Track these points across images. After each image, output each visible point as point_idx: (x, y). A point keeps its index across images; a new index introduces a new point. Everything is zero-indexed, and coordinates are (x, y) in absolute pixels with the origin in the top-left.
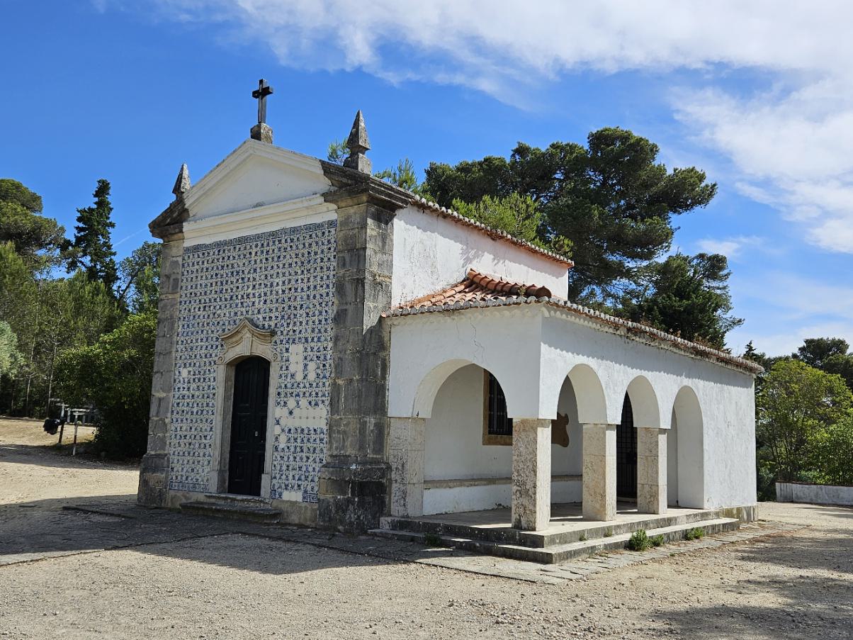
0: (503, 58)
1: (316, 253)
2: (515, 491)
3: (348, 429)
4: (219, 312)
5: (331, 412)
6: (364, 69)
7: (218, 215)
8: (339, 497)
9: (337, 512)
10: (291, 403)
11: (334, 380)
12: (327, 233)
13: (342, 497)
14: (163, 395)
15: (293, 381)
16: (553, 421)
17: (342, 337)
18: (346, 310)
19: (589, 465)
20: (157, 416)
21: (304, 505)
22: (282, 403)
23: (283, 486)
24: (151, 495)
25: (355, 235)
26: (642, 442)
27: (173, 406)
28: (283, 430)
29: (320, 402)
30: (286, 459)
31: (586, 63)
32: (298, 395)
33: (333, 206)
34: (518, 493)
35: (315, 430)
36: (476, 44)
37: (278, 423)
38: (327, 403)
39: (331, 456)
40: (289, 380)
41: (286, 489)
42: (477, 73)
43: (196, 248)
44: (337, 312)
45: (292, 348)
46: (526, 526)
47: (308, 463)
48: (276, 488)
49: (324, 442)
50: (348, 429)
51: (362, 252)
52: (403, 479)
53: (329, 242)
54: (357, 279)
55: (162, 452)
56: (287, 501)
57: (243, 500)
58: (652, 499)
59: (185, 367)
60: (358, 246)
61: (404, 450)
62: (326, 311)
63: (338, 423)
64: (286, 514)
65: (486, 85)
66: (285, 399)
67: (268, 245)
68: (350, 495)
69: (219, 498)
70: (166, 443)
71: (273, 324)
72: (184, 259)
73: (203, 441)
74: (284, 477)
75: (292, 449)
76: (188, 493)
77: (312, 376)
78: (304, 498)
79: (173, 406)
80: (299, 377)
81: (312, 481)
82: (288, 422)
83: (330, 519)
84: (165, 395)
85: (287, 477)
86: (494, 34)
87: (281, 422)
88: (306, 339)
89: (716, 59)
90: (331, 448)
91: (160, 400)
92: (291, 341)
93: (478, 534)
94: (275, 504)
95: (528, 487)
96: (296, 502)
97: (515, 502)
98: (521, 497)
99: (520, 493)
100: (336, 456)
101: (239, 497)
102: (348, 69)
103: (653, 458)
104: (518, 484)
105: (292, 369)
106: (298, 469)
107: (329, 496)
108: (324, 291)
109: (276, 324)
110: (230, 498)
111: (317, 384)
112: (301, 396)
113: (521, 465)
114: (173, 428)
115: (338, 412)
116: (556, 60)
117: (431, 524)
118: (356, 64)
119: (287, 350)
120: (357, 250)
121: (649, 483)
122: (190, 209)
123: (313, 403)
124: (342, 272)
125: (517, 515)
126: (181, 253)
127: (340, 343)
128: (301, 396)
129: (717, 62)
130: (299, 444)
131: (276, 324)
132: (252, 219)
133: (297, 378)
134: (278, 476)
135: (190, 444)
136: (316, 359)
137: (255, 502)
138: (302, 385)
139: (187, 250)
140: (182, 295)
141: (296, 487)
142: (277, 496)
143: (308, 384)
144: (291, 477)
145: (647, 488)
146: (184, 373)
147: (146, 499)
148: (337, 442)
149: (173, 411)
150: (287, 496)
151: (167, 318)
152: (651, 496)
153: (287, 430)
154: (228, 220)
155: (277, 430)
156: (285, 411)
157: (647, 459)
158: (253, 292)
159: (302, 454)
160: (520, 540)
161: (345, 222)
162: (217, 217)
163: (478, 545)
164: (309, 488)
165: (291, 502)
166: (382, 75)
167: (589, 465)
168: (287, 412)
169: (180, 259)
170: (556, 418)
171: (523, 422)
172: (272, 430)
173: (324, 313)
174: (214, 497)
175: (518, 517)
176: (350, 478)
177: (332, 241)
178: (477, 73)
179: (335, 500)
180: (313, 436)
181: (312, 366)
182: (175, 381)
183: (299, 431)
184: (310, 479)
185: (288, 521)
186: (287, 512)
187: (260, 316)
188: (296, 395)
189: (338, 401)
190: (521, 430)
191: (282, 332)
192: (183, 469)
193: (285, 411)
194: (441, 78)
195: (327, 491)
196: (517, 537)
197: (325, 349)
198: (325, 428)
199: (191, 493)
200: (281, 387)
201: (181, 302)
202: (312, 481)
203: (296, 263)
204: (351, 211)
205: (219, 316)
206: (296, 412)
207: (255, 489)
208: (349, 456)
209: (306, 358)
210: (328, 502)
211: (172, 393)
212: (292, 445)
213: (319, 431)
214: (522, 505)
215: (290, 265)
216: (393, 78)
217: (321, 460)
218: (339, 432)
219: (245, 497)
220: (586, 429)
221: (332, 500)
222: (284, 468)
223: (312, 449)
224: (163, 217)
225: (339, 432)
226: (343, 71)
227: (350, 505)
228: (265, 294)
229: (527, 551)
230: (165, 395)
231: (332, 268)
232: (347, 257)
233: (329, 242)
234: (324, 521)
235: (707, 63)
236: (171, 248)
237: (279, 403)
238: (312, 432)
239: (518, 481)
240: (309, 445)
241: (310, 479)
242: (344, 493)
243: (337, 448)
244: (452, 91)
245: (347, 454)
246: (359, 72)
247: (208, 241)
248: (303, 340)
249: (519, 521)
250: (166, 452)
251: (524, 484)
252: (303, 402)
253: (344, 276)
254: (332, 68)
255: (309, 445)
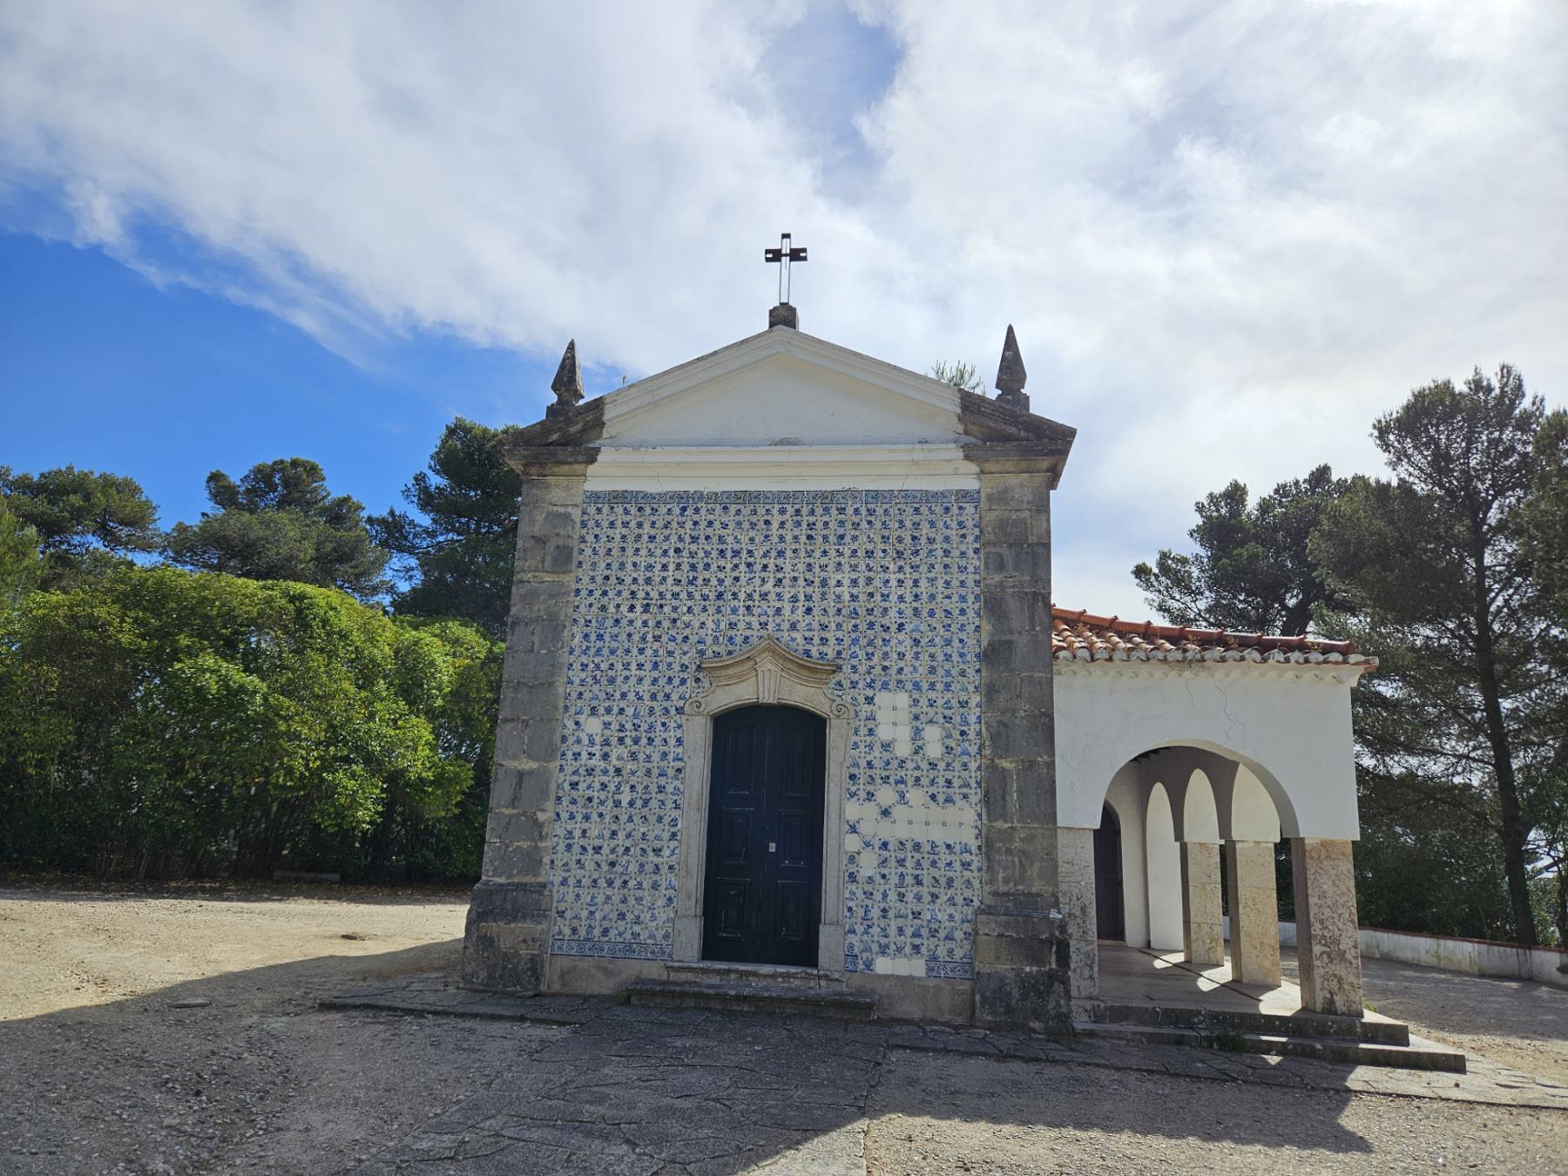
0: (332, 290)
1: (931, 541)
2: (1318, 954)
3: (1032, 848)
4: (686, 618)
5: (989, 815)
6: (105, 251)
7: (699, 446)
8: (1028, 969)
9: (1024, 997)
10: (886, 795)
11: (992, 760)
12: (955, 510)
13: (1034, 968)
14: (528, 765)
15: (887, 756)
16: (1095, 831)
17: (1004, 687)
18: (1011, 642)
19: (1250, 903)
20: (513, 803)
21: (931, 983)
22: (863, 795)
23: (875, 947)
24: (504, 968)
25: (1024, 521)
26: (1195, 864)
27: (559, 787)
28: (868, 844)
29: (957, 798)
30: (878, 896)
31: (450, 325)
32: (902, 781)
33: (973, 468)
34: (1325, 956)
35: (949, 846)
36: (297, 266)
37: (853, 829)
38: (974, 799)
39: (995, 894)
40: (877, 754)
41: (883, 953)
42: (293, 302)
43: (619, 497)
44: (990, 644)
45: (882, 698)
46: (1344, 1009)
47: (937, 906)
48: (856, 951)
49: (974, 867)
50: (1032, 848)
51: (1041, 550)
52: (1084, 933)
53: (961, 525)
54: (1034, 593)
55: (528, 879)
56: (887, 977)
57: (774, 976)
58: (1214, 944)
59: (594, 711)
60: (1033, 539)
61: (1083, 883)
62: (961, 641)
63: (1007, 836)
64: (886, 1001)
65: (305, 321)
66: (870, 788)
67: (812, 513)
68: (1054, 966)
69: (705, 971)
70: (541, 862)
71: (830, 651)
72: (584, 513)
73: (651, 857)
74: (876, 930)
75: (894, 880)
76: (610, 962)
77: (934, 750)
78: (930, 969)
79: (559, 787)
80: (903, 749)
81: (949, 938)
82: (872, 827)
83: (1009, 1010)
84: (535, 765)
85: (884, 930)
86: (324, 255)
87: (862, 828)
88: (917, 686)
89: (609, 362)
90: (992, 880)
91: (521, 775)
92: (878, 685)
93: (1280, 1026)
94: (856, 981)
95: (1342, 947)
96: (912, 978)
97: (1322, 971)
98: (1331, 962)
99: (1329, 957)
100: (1007, 894)
101: (766, 969)
102: (77, 245)
103: (1213, 886)
104: (1323, 942)
105: (884, 733)
106: (911, 916)
107: (1004, 968)
108: (954, 605)
109: (839, 653)
110: (737, 971)
111: (948, 765)
112: (910, 783)
113: (1327, 912)
114: (561, 832)
115: (1004, 816)
116: (409, 312)
117: (1181, 1011)
118: (93, 239)
119: (869, 700)
120: (1029, 545)
121: (1209, 921)
122: (608, 424)
123: (941, 798)
124: (997, 578)
125: (1326, 992)
126: (579, 500)
127: (1001, 699)
128: (910, 783)
129: (609, 365)
130: (910, 871)
131: (839, 653)
132: (780, 465)
133: (896, 751)
134: (860, 929)
135: (613, 864)
136: (941, 720)
137: (809, 977)
138: (910, 765)
139: (595, 497)
140: (580, 577)
141: (908, 949)
142: (861, 966)
143: (925, 762)
144: (893, 930)
145: (1206, 929)
146: (593, 726)
147: (490, 976)
148: (1006, 868)
149: (559, 798)
150: (883, 966)
151: (538, 619)
152: (1212, 940)
153: (877, 844)
154: (783, 457)
155: (852, 843)
156: (871, 810)
157: (1204, 888)
158: (778, 590)
159: (920, 888)
160: (1365, 1034)
161: (999, 498)
162: (695, 449)
163: (1318, 1046)
164: (942, 952)
165: (899, 978)
166: (137, 266)
167: (1250, 903)
168: (877, 811)
169: (576, 514)
170: (1358, 839)
171: (1325, 844)
172: (838, 844)
173: (956, 643)
174: (691, 969)
175: (1329, 996)
176: (1052, 935)
177: (970, 524)
178: (293, 302)
179: (1018, 975)
180: (945, 857)
181: (932, 734)
182: (564, 739)
183: (909, 846)
184: (942, 934)
185: (893, 1014)
186: (889, 997)
187: (797, 635)
188: (897, 782)
189: (1003, 798)
190: (1323, 857)
191: (854, 667)
192: (592, 913)
193: (871, 810)
194: (235, 294)
195: (998, 958)
196: (1359, 1030)
197: (964, 704)
198: (974, 844)
199: (621, 963)
200: (856, 765)
201: (578, 591)
202: (949, 938)
203: (795, 551)
204: (1013, 480)
205: (687, 625)
206: (899, 812)
207: (807, 954)
208: (1038, 895)
209: (916, 718)
210: (1002, 979)
211: (558, 763)
212: (893, 871)
213: (957, 849)
214: (1335, 976)
215: (869, 554)
216: (155, 275)
217: (970, 901)
218: (1009, 851)
219: (781, 969)
220: (1243, 849)
221: (1011, 975)
222: (875, 913)
223: (943, 881)
224: (543, 428)
225: (1009, 851)
226: (67, 245)
227: (1056, 985)
228: (808, 598)
229: (1391, 1051)
230: (535, 765)
231: (971, 569)
232: (1008, 556)
233: (961, 525)
234: (993, 1013)
235: (598, 363)
236: (547, 487)
237: (853, 795)
238: (943, 849)
239: (1324, 937)
240: (935, 872)
241: (942, 934)
242: (1041, 962)
243: (1006, 881)
244: (261, 316)
245: (1034, 890)
246: (96, 253)
247: (652, 488)
248: (909, 686)
249: (1332, 1001)
250: (540, 880)
251: (1336, 942)
252: (915, 795)
253: (1001, 585)
254: (47, 234)
255: (935, 872)
